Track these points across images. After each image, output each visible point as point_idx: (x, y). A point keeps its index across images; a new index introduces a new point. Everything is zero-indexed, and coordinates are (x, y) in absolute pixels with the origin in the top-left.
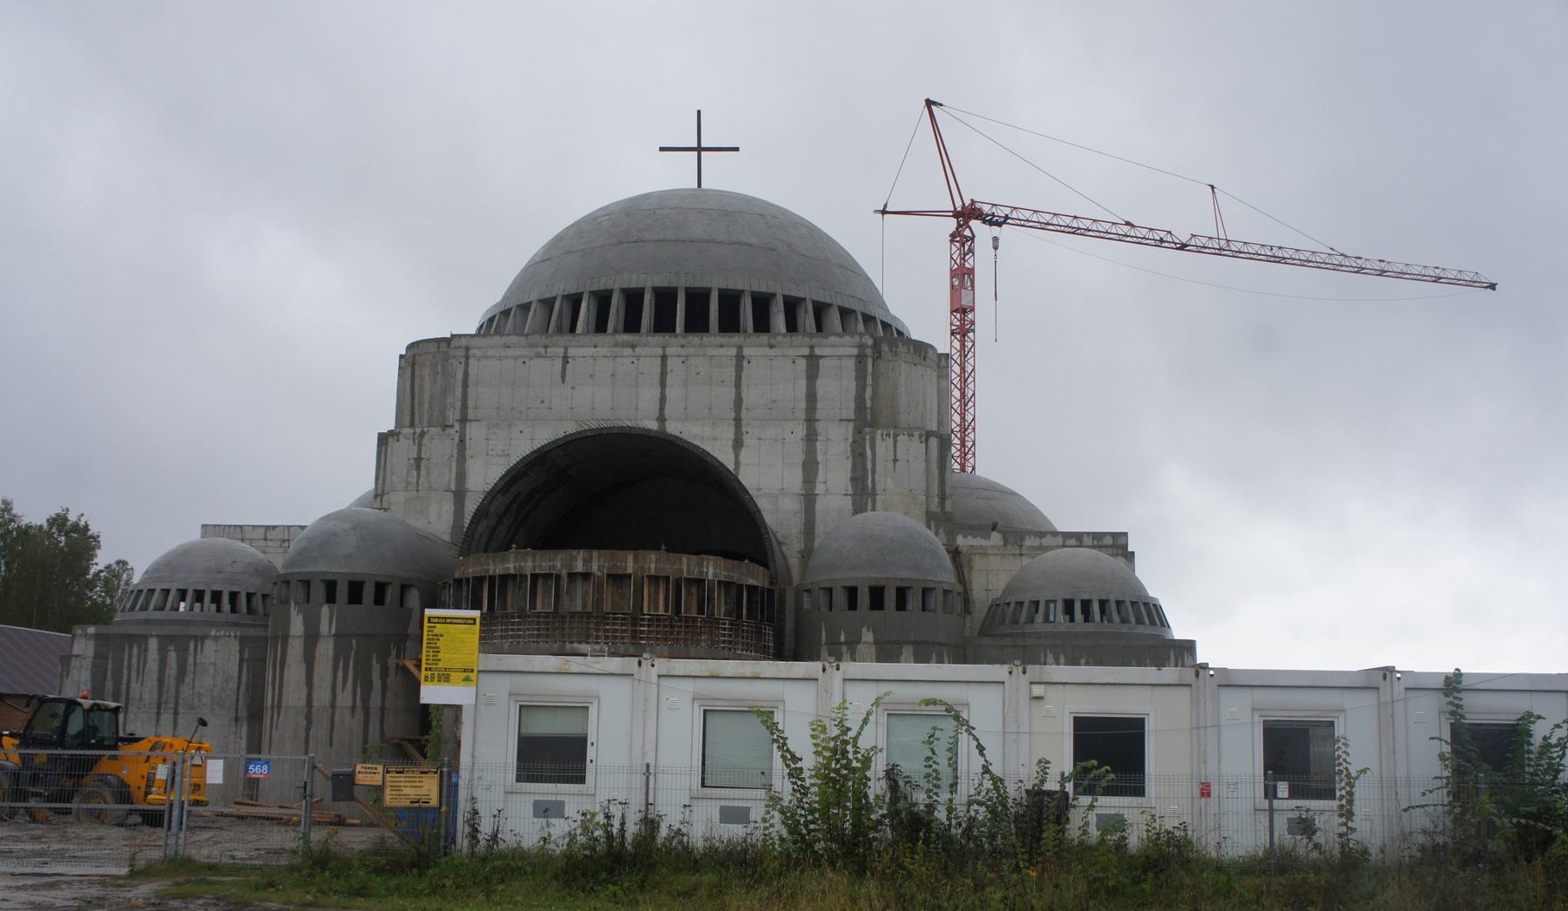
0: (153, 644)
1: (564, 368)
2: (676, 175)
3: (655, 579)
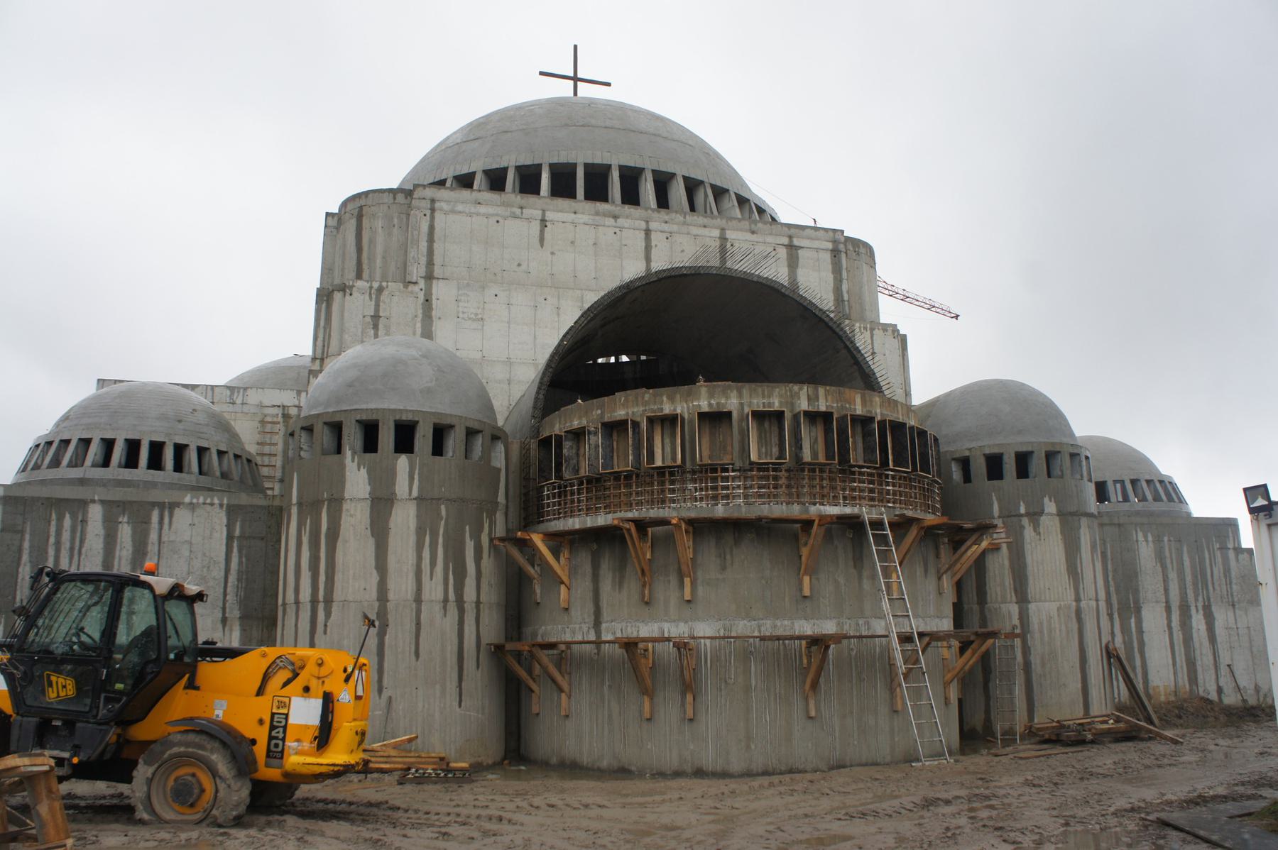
0: (95, 513)
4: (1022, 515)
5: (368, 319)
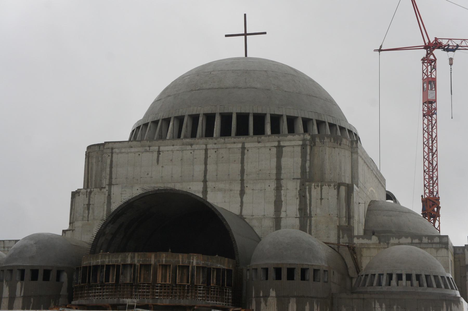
1: (158, 157)
2: (233, 50)
3: (165, 267)
4: (261, 297)
5: (86, 206)
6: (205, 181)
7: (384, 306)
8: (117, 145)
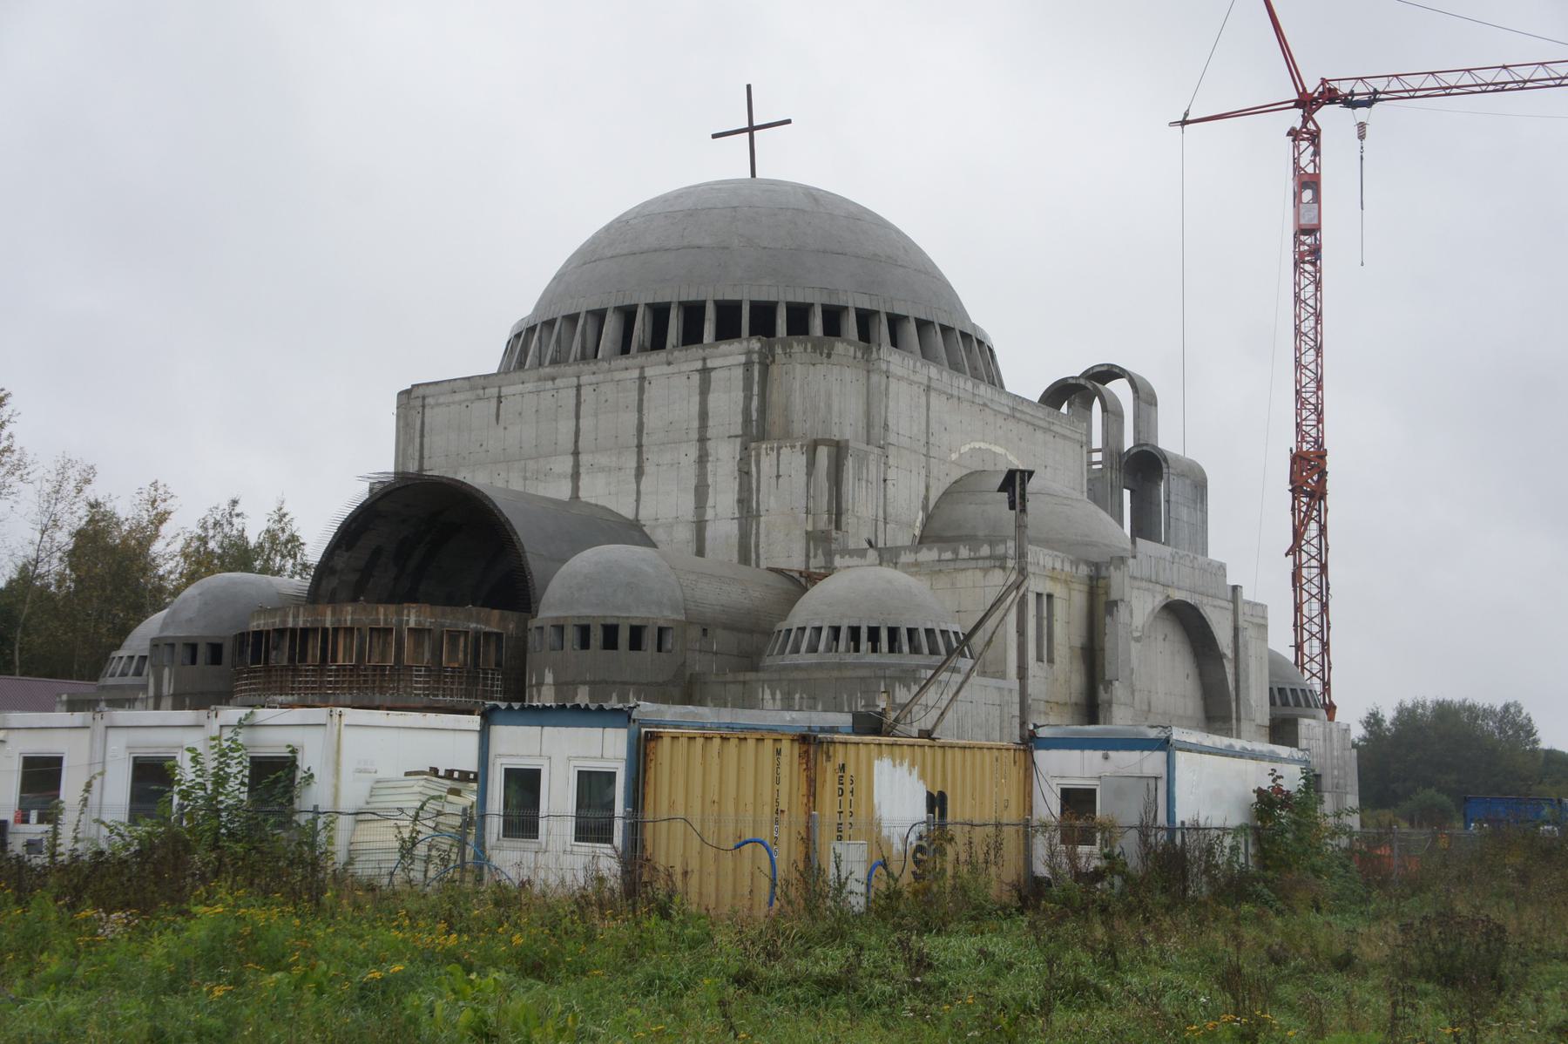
2: (728, 163)
3: (349, 631)
6: (576, 453)
7: (778, 696)
8: (428, 391)
